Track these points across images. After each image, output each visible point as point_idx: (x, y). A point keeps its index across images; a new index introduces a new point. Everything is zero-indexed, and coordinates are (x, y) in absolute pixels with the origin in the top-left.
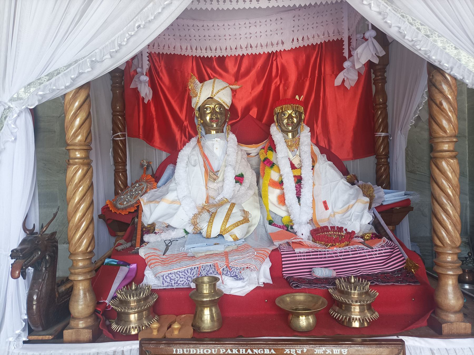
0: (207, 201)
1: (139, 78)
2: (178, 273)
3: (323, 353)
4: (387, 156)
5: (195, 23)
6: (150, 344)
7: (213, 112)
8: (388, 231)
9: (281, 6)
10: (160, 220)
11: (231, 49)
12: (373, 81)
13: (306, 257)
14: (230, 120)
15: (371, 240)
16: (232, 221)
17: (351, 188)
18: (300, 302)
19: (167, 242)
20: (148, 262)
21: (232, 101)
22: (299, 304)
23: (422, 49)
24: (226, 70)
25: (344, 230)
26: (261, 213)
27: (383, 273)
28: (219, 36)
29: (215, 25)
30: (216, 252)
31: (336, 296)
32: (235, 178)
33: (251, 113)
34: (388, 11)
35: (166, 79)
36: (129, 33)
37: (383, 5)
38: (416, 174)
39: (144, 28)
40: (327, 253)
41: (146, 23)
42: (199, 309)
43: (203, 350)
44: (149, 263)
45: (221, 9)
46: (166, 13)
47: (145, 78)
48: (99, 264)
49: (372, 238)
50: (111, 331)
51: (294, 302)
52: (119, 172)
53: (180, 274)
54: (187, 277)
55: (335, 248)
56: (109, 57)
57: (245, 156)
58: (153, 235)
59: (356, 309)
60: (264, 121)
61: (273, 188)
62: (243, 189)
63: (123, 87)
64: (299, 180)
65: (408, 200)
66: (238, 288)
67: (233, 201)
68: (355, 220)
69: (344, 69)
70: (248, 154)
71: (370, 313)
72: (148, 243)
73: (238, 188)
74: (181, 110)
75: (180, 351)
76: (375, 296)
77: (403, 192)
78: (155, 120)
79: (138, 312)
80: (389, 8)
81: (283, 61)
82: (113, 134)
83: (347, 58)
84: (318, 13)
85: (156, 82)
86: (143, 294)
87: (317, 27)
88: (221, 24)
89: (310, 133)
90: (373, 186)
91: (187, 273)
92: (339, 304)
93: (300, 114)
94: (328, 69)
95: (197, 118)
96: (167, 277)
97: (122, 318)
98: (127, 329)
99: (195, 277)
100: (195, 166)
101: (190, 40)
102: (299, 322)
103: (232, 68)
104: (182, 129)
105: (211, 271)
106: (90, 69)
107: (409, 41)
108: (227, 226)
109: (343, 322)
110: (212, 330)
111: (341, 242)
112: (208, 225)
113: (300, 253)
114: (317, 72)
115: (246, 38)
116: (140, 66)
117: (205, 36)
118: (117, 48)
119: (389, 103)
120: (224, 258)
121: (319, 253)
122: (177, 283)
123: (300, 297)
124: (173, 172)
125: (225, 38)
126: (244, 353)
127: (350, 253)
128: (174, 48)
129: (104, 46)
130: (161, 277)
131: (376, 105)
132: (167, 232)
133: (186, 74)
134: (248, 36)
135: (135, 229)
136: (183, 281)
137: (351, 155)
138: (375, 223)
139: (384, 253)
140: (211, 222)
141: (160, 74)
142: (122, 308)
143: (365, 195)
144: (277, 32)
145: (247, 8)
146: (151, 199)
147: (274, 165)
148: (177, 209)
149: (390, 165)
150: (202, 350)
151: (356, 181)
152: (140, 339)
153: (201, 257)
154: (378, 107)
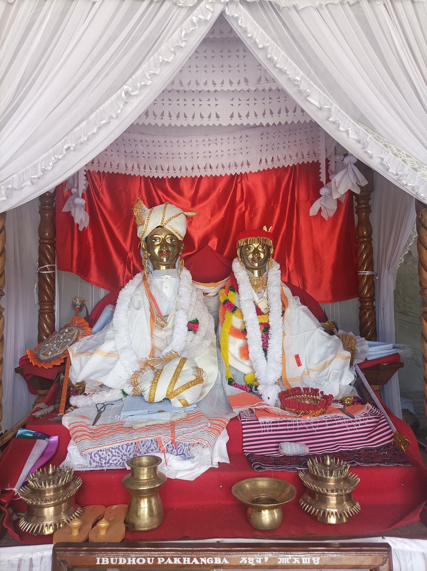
0: (152, 355)
1: (73, 200)
2: (111, 449)
3: (288, 562)
4: (372, 298)
5: (144, 138)
6: (66, 551)
7: (163, 243)
8: (373, 395)
9: (245, 124)
10: (92, 378)
11: (187, 169)
12: (355, 210)
13: (272, 428)
14: (184, 252)
15: (352, 406)
16: (181, 382)
17: (329, 339)
18: (263, 490)
19: (99, 406)
20: (72, 435)
21: (187, 231)
22: (262, 493)
23: (408, 185)
24: (181, 193)
25: (319, 392)
26: (219, 369)
27: (366, 450)
28: (173, 154)
29: (168, 141)
30: (160, 422)
31: (308, 483)
32: (188, 326)
33: (210, 244)
34: (368, 139)
35: (107, 200)
36: (56, 156)
37: (363, 132)
38: (409, 315)
39: (74, 150)
40: (298, 423)
41: (76, 145)
42: (135, 500)
43: (136, 560)
44: (74, 436)
45: (173, 125)
46: (104, 133)
47: (81, 201)
48: (9, 436)
49: (353, 403)
50: (18, 530)
51: (256, 489)
52: (45, 313)
53: (113, 451)
54: (122, 455)
55: (308, 418)
56: (30, 183)
57: (202, 297)
58: (83, 396)
59: (333, 500)
60: (225, 253)
61: (235, 337)
62: (197, 338)
63: (54, 209)
64: (266, 328)
65: (397, 354)
66: (186, 470)
67: (184, 355)
68: (334, 380)
69: (321, 196)
70: (205, 294)
71: (350, 506)
72: (76, 407)
73: (191, 338)
74: (125, 239)
75: (105, 561)
76: (355, 483)
77: (391, 345)
78: (92, 250)
79: (54, 505)
80: (370, 136)
81: (250, 183)
82: (39, 266)
83: (324, 183)
84: (290, 130)
85: (96, 204)
86: (62, 481)
87: (289, 146)
88: (174, 140)
89: (280, 271)
90: (355, 337)
91: (121, 449)
92: (312, 493)
93: (268, 248)
94: (302, 194)
95: (144, 250)
96: (97, 455)
97: (33, 513)
98: (39, 527)
99: (131, 457)
100: (138, 309)
101: (138, 157)
102: (261, 517)
103: (188, 192)
104: (126, 262)
105: (152, 447)
106: (4, 198)
107: (394, 175)
108: (175, 388)
109: (316, 517)
110: (150, 528)
111: (315, 408)
112: (151, 386)
113: (265, 423)
114: (289, 198)
115: (205, 157)
116: (76, 186)
117: (155, 153)
118: (40, 174)
119: (374, 236)
120: (170, 431)
121: (288, 423)
122: (108, 462)
123: (263, 483)
124: (111, 317)
125: (180, 156)
126: (189, 563)
127: (327, 423)
128: (118, 166)
129: (24, 170)
130: (88, 455)
131: (360, 238)
132: (100, 393)
133: (133, 196)
134: (207, 155)
135: (60, 388)
136: (116, 460)
137: (330, 297)
138: (357, 384)
139: (368, 423)
140: (155, 382)
141: (101, 195)
142: (34, 500)
143: (346, 348)
144: (241, 151)
145: (205, 125)
146: (82, 350)
147: (236, 310)
148: (114, 364)
149: (376, 310)
150: (134, 559)
151: (335, 330)
152: (54, 543)
153: (140, 428)
154: (362, 240)
